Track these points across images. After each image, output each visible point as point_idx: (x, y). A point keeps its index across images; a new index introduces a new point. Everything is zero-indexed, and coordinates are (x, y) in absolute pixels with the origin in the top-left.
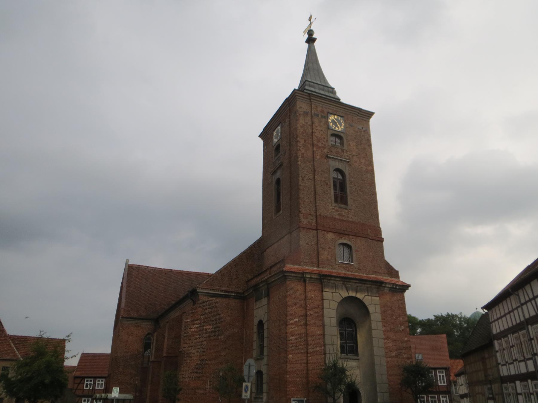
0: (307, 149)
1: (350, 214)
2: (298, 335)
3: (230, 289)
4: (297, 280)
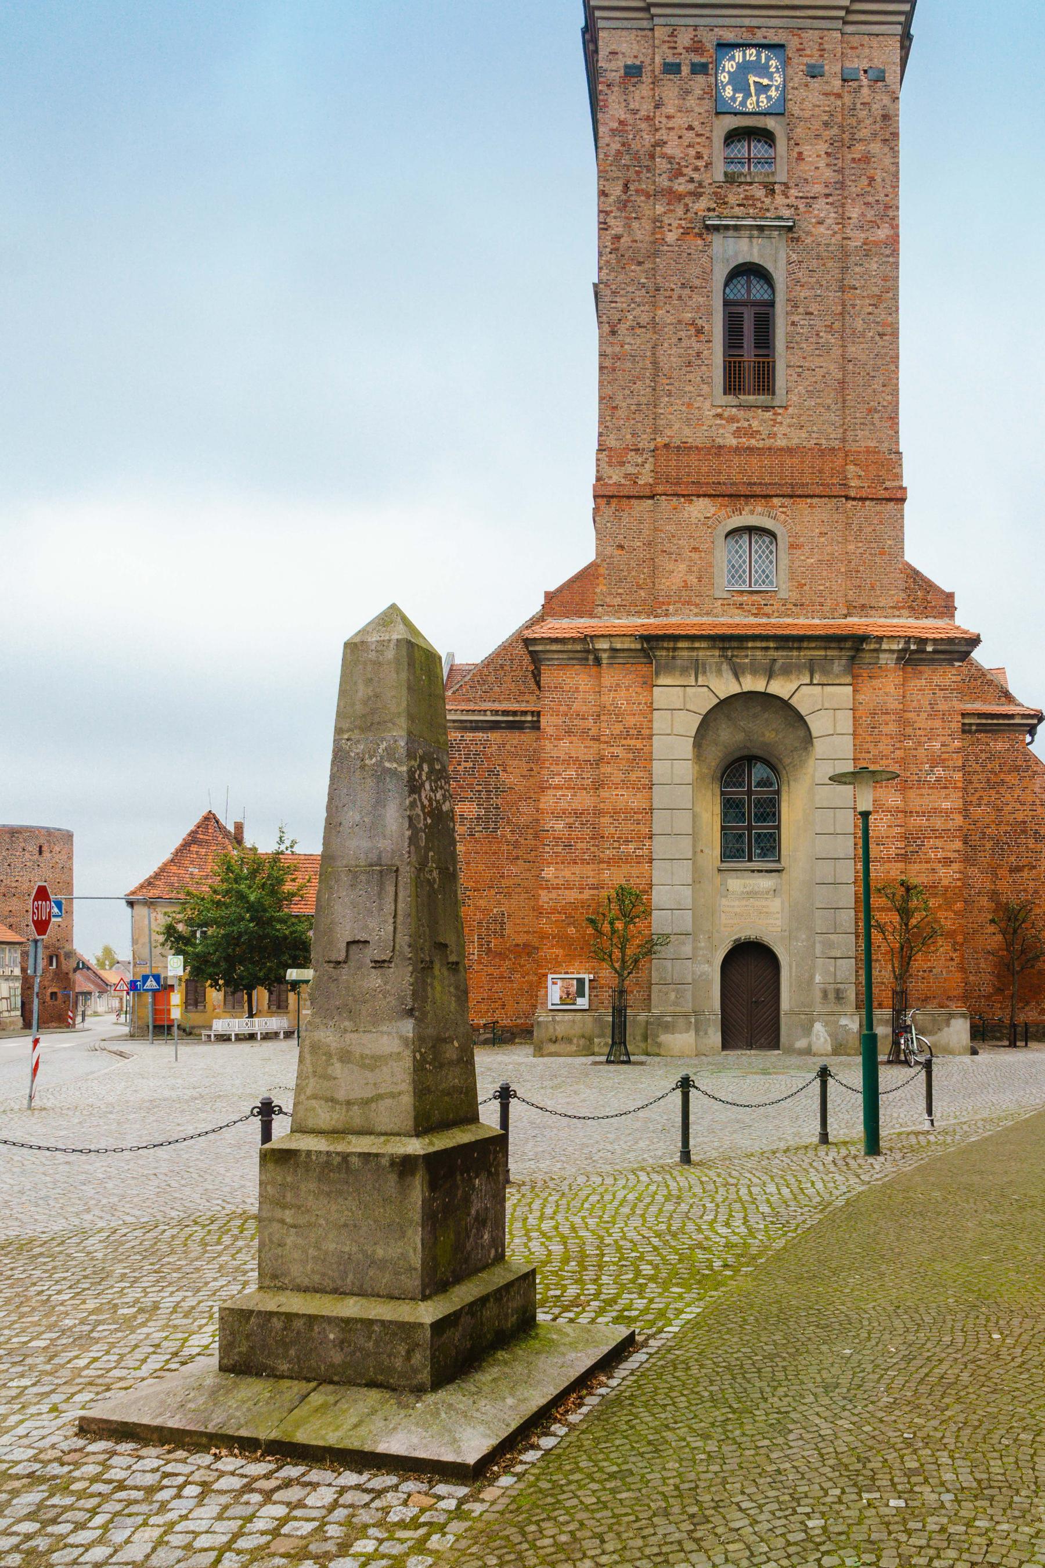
0: (634, 215)
1: (781, 423)
2: (576, 813)
3: (523, 707)
4: (574, 662)
